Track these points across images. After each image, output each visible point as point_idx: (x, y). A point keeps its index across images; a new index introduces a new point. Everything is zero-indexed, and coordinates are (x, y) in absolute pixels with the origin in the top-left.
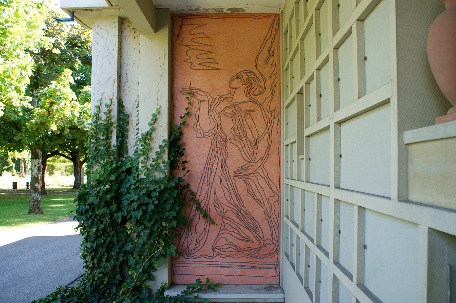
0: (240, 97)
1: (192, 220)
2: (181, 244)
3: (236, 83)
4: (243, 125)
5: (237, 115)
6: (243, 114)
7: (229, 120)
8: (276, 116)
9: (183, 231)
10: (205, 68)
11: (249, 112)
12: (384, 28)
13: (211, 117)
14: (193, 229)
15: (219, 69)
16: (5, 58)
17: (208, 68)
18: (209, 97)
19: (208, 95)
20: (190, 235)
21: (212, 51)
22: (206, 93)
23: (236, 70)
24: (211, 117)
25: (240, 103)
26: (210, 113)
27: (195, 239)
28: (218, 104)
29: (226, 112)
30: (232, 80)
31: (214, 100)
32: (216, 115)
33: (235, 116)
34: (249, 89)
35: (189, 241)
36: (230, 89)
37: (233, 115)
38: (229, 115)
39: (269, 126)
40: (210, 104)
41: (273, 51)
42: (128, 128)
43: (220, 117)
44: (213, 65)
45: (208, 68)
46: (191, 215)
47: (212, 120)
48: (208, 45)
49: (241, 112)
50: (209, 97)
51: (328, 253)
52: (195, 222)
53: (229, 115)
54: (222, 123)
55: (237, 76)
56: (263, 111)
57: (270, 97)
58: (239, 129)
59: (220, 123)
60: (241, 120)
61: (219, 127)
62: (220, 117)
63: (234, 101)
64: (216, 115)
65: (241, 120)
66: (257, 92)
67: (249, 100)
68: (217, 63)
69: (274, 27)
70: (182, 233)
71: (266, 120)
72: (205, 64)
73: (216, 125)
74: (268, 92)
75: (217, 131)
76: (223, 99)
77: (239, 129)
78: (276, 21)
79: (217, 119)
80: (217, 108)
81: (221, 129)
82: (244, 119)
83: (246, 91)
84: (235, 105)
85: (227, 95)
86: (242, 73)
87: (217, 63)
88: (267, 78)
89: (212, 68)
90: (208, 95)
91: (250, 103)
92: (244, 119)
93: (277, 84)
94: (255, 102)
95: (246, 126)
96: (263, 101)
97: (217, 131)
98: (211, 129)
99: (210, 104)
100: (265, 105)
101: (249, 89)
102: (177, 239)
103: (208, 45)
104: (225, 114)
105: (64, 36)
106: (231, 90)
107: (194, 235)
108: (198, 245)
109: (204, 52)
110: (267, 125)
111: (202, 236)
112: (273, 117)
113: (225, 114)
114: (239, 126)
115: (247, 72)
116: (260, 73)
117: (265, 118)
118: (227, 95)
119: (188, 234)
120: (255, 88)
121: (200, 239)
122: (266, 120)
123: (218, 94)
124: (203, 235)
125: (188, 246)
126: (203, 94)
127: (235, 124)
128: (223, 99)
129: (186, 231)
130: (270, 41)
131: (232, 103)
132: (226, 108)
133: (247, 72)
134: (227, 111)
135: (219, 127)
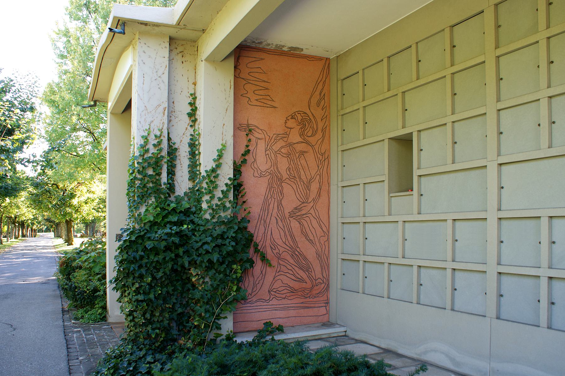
0: (295, 137)
3: (291, 123)
6: (297, 155)
7: (285, 160)
10: (262, 104)
11: (302, 153)
15: (276, 107)
17: (265, 105)
19: (265, 133)
32: (272, 154)
34: (303, 130)
37: (288, 155)
38: (285, 155)
43: (276, 157)
44: (270, 103)
47: (268, 159)
48: (265, 81)
53: (285, 155)
58: (294, 169)
62: (276, 157)
63: (289, 141)
64: (272, 154)
66: (309, 134)
74: (319, 135)
77: (294, 169)
78: (327, 65)
79: (274, 158)
80: (274, 147)
81: (277, 168)
84: (290, 145)
86: (296, 113)
88: (319, 120)
90: (265, 133)
94: (307, 143)
95: (300, 167)
100: (316, 147)
101: (303, 130)
103: (265, 81)
106: (287, 130)
112: (323, 159)
116: (313, 114)
120: (309, 129)
126: (260, 132)
127: (290, 164)
130: (321, 84)
132: (282, 147)
134: (283, 150)
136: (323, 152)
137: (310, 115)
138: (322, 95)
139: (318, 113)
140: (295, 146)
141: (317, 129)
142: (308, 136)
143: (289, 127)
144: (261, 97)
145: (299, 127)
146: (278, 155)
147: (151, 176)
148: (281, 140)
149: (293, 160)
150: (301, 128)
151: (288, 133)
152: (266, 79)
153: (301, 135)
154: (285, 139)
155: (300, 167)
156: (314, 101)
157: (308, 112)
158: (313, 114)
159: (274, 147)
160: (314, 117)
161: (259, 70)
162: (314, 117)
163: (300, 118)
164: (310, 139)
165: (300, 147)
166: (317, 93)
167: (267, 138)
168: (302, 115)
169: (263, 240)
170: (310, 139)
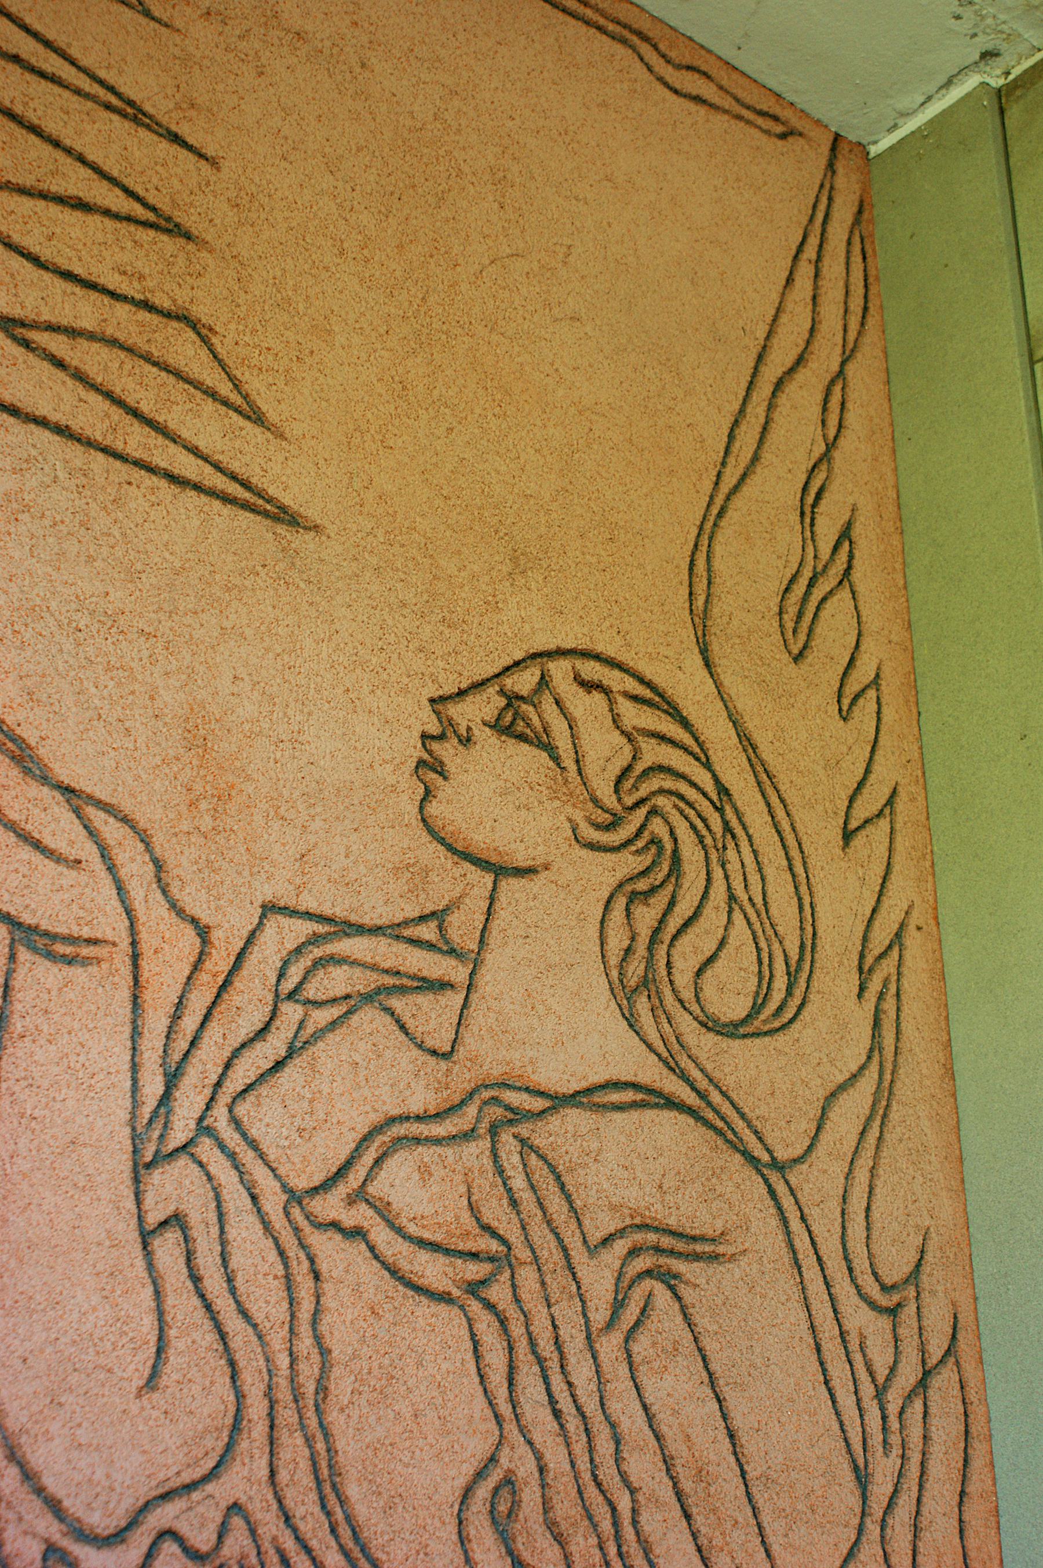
0: (551, 1008)
3: (497, 792)
4: (605, 1447)
5: (528, 1276)
6: (599, 1278)
7: (436, 1339)
8: (936, 1352)
10: (92, 416)
11: (666, 1253)
13: (168, 1249)
15: (283, 516)
16: (447, 751)
17: (136, 440)
18: (152, 911)
19: (135, 866)
21: (189, 221)
22: (111, 830)
23: (493, 605)
24: (168, 1249)
25: (560, 1101)
26: (174, 1187)
28: (275, 1046)
29: (383, 1210)
30: (447, 731)
31: (219, 962)
32: (244, 1228)
33: (499, 1293)
34: (646, 916)
36: (432, 852)
37: (481, 1273)
38: (433, 1270)
39: (881, 1489)
40: (156, 1022)
41: (846, 534)
43: (301, 1277)
44: (207, 426)
45: (136, 440)
47: (182, 1304)
48: (134, 113)
49: (574, 1243)
50: (152, 911)
53: (433, 1270)
54: (341, 1385)
55: (513, 699)
56: (812, 1273)
57: (867, 1084)
58: (566, 1508)
59: (309, 1371)
60: (582, 1373)
61: (293, 1448)
62: (301, 1277)
63: (487, 1053)
64: (244, 1228)
65: (582, 1373)
66: (730, 993)
67: (651, 1072)
68: (256, 417)
69: (833, 268)
71: (847, 1401)
72: (92, 358)
73: (256, 1409)
74: (833, 1026)
75: (271, 1526)
76: (337, 981)
77: (566, 1508)
78: (843, 214)
79: (268, 1304)
80: (268, 1117)
81: (328, 1482)
82: (609, 1346)
83: (617, 941)
84: (506, 1111)
85: (392, 931)
86: (560, 670)
87: (256, 417)
88: (820, 832)
89: (188, 466)
90: (135, 866)
91: (668, 1124)
92: (609, 1346)
93: (913, 940)
94: (710, 1111)
95: (643, 1467)
96: (805, 1126)
97: (271, 1526)
98: (175, 1467)
99: (156, 1022)
100: (819, 1182)
101: (646, 916)
103: (134, 113)
104: (381, 1235)
105: (427, 1357)
106: (451, 881)
109: (76, 181)
110: (862, 1478)
112: (909, 1374)
113: (381, 1235)
114: (556, 1458)
115: (613, 678)
116: (747, 742)
117: (838, 1371)
118: (392, 931)
120: (714, 918)
122: (847, 1401)
123: (280, 890)
126: (59, 826)
127: (506, 1416)
128: (337, 981)
130: (804, 395)
131: (462, 1079)
132: (389, 1135)
133: (613, 678)
134: (401, 1181)
135: (293, 1448)
136: (895, 1270)
137: (718, 733)
138: (827, 531)
139: (810, 747)
140: (566, 1133)
141: (809, 946)
142: (709, 1024)
143: (480, 839)
144: (85, 310)
145: (608, 871)
146: (328, 1248)
147: (28, 1493)
148: (370, 1020)
149: (552, 1364)
150: (631, 893)
151: (463, 928)
152: (139, 84)
153: (638, 988)
154: (433, 1016)
155: (643, 1467)
156: (757, 559)
157: (690, 687)
158: (747, 742)
159: (268, 1117)
160: (764, 777)
161: (184, 349)
162: (764, 777)
163: (603, 750)
164: (744, 1068)
165: (632, 1166)
166: (777, 485)
167: (170, 953)
168: (633, 715)
169: (817, 594)
170: (744, 1068)
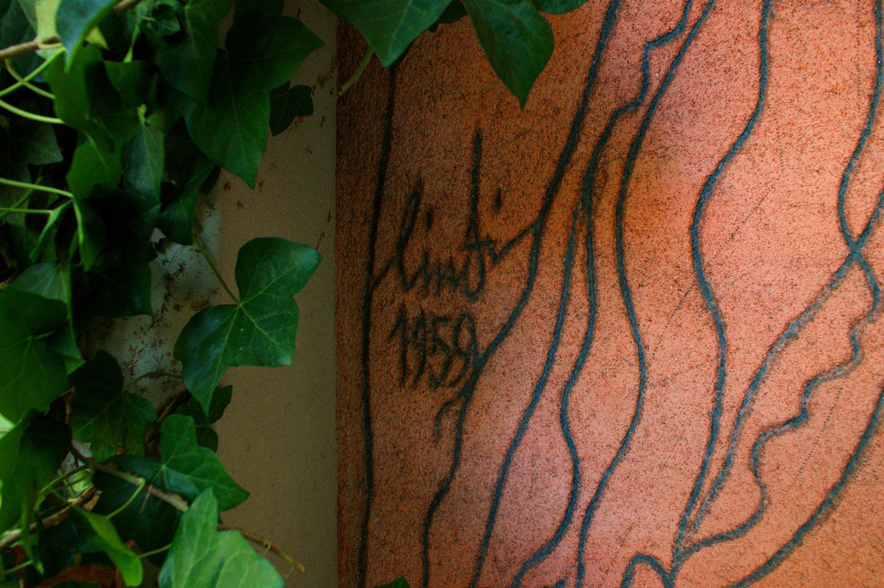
1: (646, 103)
2: (477, 474)
9: (504, 282)
12: (639, 516)
14: (659, 248)
20: (613, 342)
27: (682, 402)
35: (599, 432)
42: (824, 305)
46: (629, 35)
51: (257, 241)
52: (694, 136)
70: (491, 311)
102: (426, 402)
107: (679, 346)
108: (731, 505)
111: (797, 363)
119: (575, 326)
121: (773, 406)
124: (827, 338)
125: (578, 514)
129: (548, 282)
